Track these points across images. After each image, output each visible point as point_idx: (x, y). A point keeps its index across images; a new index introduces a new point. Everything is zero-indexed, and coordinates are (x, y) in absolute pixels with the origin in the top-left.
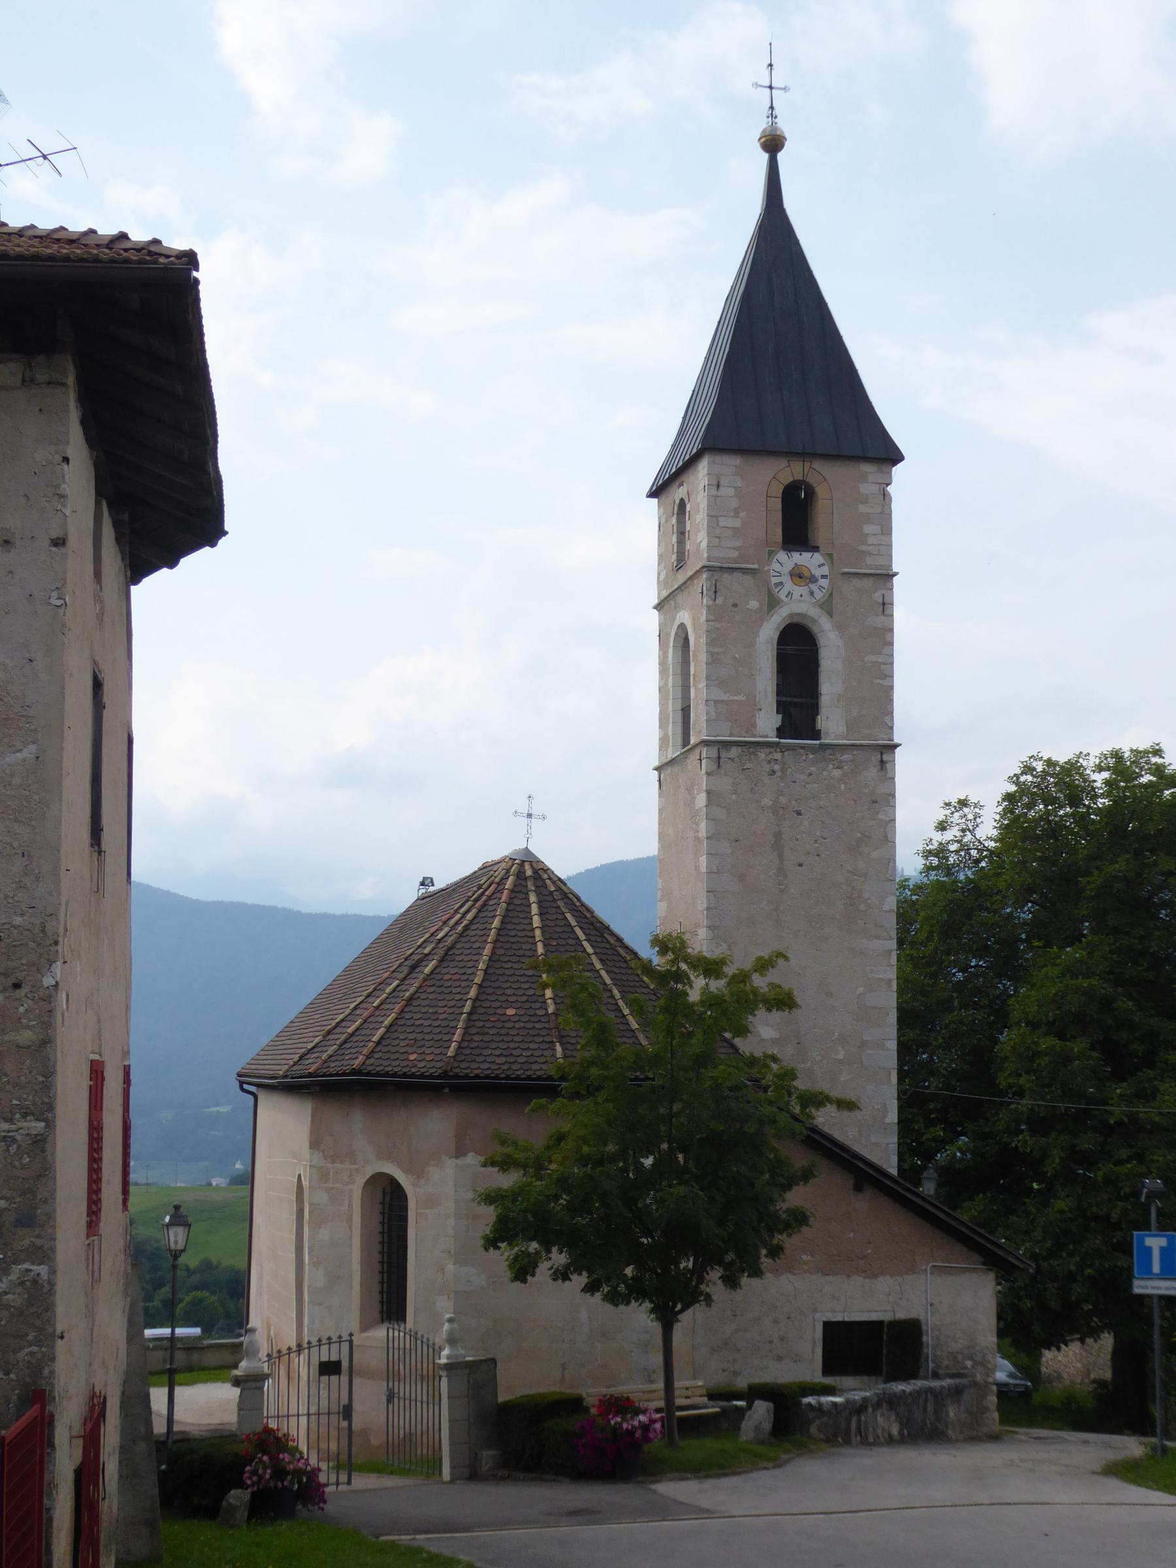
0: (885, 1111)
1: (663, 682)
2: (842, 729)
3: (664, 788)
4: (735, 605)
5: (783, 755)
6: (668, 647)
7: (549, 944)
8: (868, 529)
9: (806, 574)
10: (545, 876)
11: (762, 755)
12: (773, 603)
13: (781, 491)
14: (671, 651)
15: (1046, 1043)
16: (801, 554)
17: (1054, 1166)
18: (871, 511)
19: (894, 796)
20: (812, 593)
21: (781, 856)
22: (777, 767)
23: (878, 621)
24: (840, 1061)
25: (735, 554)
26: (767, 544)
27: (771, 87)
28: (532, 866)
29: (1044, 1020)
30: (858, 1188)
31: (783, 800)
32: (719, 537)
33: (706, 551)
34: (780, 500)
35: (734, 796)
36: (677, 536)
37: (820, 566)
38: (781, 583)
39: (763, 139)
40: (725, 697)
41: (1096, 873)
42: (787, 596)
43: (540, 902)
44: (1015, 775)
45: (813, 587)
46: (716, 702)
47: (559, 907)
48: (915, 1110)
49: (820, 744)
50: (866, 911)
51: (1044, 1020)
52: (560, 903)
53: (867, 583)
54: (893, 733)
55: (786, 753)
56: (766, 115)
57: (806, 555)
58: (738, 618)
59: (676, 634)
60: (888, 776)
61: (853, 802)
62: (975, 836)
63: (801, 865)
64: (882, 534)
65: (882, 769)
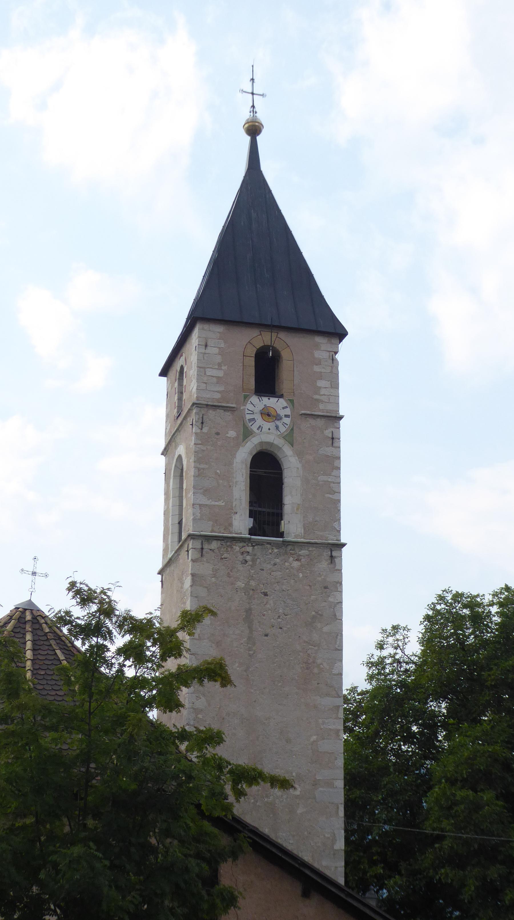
0: (334, 840)
1: (166, 507)
2: (300, 530)
3: (164, 586)
4: (218, 434)
5: (253, 548)
6: (170, 478)
7: (37, 673)
8: (321, 383)
9: (273, 413)
10: (42, 621)
11: (237, 548)
12: (247, 434)
13: (255, 353)
14: (172, 480)
15: (461, 794)
16: (269, 399)
17: (470, 893)
18: (323, 370)
19: (341, 584)
20: (277, 427)
21: (250, 628)
22: (248, 558)
23: (329, 451)
24: (297, 797)
25: (218, 396)
26: (243, 390)
27: (253, 94)
28: (32, 613)
29: (460, 778)
30: (306, 894)
31: (253, 583)
32: (206, 383)
33: (196, 393)
34: (253, 359)
35: (213, 579)
36: (178, 395)
37: (283, 408)
38: (254, 419)
39: (246, 126)
40: (208, 502)
41: (495, 668)
42: (258, 429)
43: (34, 640)
44: (432, 603)
45: (278, 423)
46: (200, 505)
47: (51, 645)
48: (362, 854)
49: (283, 541)
50: (319, 674)
51: (460, 778)
52: (53, 642)
53: (320, 422)
54: (340, 535)
55: (256, 547)
56: (249, 111)
57: (273, 400)
58: (219, 443)
59: (175, 466)
60: (337, 568)
61: (308, 588)
62: (404, 653)
63: (266, 635)
64: (332, 387)
65: (331, 562)
